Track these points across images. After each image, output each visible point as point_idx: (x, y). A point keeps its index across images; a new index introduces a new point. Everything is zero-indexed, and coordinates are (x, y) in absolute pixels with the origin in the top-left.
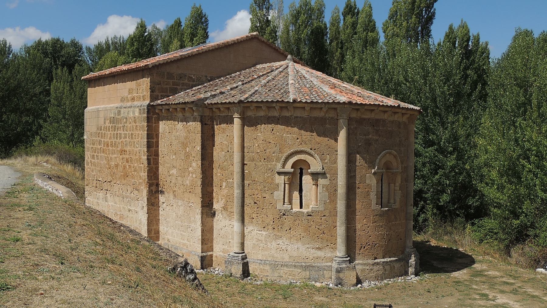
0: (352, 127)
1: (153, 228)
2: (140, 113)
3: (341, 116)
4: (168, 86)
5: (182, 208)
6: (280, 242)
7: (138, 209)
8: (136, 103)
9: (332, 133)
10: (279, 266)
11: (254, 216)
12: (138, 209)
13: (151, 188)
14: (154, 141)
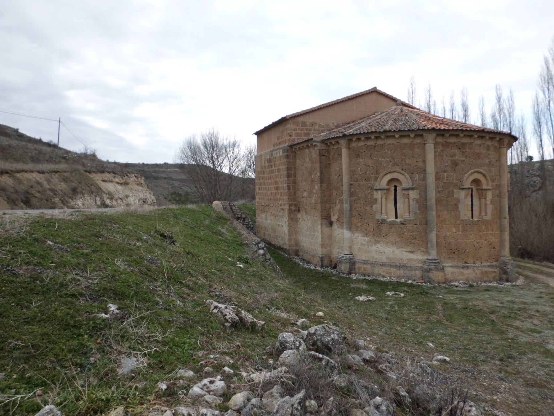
0: (439, 150)
2: (283, 153)
4: (302, 132)
5: (310, 221)
6: (378, 245)
7: (283, 224)
8: (282, 146)
11: (359, 225)
12: (283, 224)
14: (293, 172)
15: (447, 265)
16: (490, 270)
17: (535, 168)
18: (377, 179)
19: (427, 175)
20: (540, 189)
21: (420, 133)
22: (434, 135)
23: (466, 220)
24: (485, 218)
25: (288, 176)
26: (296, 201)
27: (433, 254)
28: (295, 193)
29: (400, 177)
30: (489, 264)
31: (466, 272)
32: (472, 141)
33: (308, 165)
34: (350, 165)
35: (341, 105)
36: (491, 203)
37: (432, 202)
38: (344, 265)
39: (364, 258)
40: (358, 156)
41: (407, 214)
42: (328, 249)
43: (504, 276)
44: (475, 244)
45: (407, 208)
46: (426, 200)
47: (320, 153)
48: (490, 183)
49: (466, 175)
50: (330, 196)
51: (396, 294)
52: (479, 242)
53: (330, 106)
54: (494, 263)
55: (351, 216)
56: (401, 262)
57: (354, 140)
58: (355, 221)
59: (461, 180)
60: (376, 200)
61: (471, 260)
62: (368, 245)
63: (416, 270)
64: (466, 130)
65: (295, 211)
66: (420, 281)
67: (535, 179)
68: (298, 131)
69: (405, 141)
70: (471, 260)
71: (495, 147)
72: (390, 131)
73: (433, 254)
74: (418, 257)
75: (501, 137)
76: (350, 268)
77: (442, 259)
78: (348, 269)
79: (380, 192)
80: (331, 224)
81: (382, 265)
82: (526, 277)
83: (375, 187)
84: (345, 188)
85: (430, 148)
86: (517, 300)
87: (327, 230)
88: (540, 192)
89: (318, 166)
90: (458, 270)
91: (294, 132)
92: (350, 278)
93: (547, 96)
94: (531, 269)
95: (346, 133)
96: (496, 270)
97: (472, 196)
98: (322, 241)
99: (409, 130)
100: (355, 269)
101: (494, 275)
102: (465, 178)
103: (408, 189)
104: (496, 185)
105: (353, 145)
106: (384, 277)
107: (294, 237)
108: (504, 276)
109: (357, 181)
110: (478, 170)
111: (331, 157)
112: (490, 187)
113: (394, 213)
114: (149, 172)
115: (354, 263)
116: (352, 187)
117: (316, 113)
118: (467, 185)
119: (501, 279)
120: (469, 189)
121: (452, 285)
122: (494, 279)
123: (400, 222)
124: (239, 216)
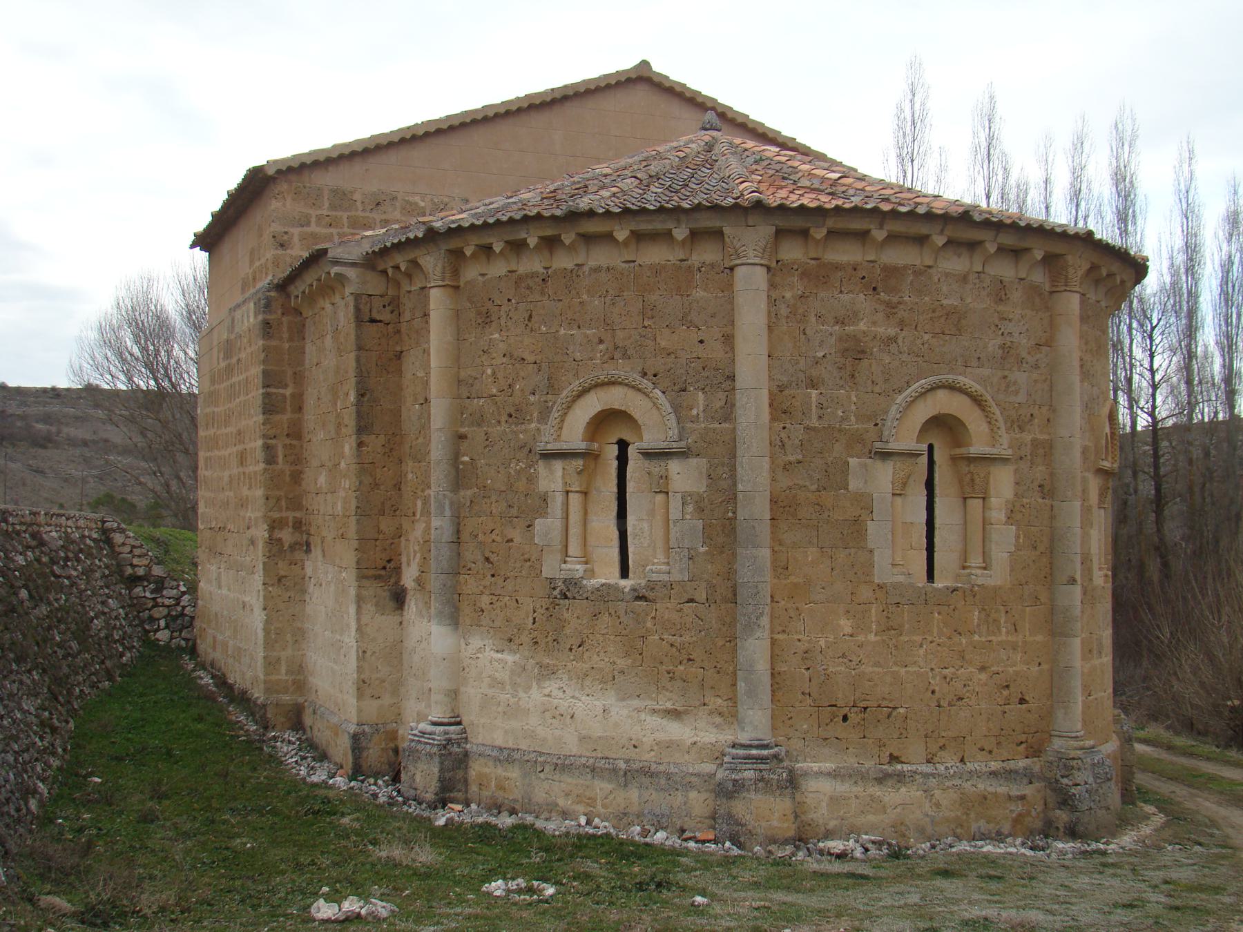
0: (788, 295)
1: (284, 655)
4: (334, 231)
6: (551, 686)
10: (547, 768)
13: (278, 534)
14: (288, 392)
15: (815, 766)
16: (1002, 790)
21: (710, 221)
23: (895, 586)
24: (981, 578)
25: (270, 407)
27: (756, 723)
28: (297, 477)
30: (994, 765)
31: (893, 796)
32: (929, 262)
33: (330, 361)
34: (457, 358)
35: (504, 128)
36: (1010, 519)
37: (755, 509)
38: (422, 766)
40: (486, 319)
41: (661, 557)
42: (387, 700)
44: (936, 683)
47: (358, 310)
50: (398, 486)
51: (530, 890)
53: (452, 128)
54: (1022, 763)
55: (457, 569)
56: (632, 753)
57: (468, 252)
60: (545, 499)
61: (915, 750)
62: (514, 685)
63: (690, 786)
64: (894, 214)
65: (292, 547)
68: (313, 228)
69: (655, 255)
70: (915, 750)
71: (1034, 289)
72: (591, 213)
73: (756, 723)
74: (693, 737)
75: (1058, 248)
76: (441, 780)
77: (796, 744)
78: (434, 785)
79: (558, 465)
80: (399, 598)
81: (563, 766)
83: (540, 447)
84: (438, 450)
85: (751, 283)
87: (383, 622)
90: (857, 789)
91: (296, 231)
92: (430, 820)
95: (438, 225)
97: (930, 485)
98: (360, 669)
99: (661, 210)
100: (466, 782)
101: (1018, 808)
103: (665, 454)
104: (1035, 443)
105: (471, 273)
106: (565, 815)
107: (289, 652)
110: (951, 377)
111: (404, 327)
112: (1002, 449)
114: (23, 417)
116: (464, 445)
117: (393, 157)
118: (906, 438)
121: (821, 852)
124: (141, 572)
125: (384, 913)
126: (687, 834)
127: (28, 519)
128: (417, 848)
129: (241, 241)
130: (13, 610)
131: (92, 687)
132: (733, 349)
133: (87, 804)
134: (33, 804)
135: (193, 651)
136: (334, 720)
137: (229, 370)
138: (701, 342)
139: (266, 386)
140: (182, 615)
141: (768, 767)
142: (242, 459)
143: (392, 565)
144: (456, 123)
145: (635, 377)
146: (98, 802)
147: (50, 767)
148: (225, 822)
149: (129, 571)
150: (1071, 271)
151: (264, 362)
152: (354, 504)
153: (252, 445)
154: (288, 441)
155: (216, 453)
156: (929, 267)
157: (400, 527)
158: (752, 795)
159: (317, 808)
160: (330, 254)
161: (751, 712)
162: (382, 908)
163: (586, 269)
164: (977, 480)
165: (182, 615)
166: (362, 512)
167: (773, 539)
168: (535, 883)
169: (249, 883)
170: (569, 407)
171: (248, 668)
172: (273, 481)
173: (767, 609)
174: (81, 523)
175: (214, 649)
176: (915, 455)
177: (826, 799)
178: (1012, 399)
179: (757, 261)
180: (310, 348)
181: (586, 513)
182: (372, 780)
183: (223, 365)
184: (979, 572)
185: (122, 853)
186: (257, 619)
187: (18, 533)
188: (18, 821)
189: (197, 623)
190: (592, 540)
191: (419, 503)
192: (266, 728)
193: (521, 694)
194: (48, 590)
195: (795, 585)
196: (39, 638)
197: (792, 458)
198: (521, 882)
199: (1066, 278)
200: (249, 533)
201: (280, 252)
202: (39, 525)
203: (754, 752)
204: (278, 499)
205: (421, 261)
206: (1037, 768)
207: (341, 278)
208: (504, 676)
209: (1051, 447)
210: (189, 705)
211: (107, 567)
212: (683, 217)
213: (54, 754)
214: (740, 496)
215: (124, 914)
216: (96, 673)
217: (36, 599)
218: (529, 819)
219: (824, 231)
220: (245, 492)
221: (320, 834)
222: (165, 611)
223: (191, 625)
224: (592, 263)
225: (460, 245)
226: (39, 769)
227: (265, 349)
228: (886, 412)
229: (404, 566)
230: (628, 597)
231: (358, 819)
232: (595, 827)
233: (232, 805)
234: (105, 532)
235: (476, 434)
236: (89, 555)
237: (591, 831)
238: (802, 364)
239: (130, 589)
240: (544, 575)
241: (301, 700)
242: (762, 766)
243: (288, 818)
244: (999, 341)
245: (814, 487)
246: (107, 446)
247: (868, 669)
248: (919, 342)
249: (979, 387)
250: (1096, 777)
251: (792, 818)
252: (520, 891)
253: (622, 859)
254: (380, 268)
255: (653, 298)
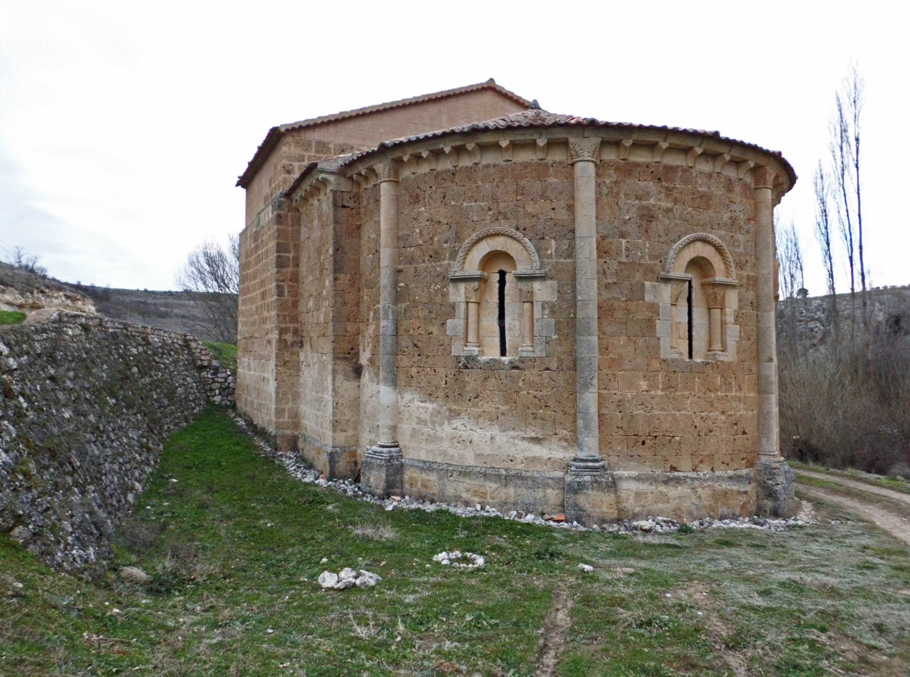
0: (608, 181)
1: (287, 407)
3: (578, 156)
6: (457, 423)
9: (561, 193)
10: (455, 474)
11: (414, 371)
13: (284, 337)
14: (291, 255)
16: (735, 488)
17: (813, 307)
18: (456, 252)
19: (578, 241)
20: (822, 341)
22: (595, 140)
23: (673, 361)
25: (281, 264)
26: (296, 321)
27: (591, 446)
28: (295, 304)
29: (512, 248)
30: (731, 473)
31: (673, 492)
32: (691, 164)
36: (736, 321)
37: (589, 312)
38: (374, 472)
39: (423, 456)
40: (416, 200)
41: (528, 342)
43: (768, 502)
44: (697, 422)
45: (528, 328)
46: (575, 305)
47: (335, 200)
48: (734, 272)
49: (675, 246)
50: (358, 304)
51: (465, 560)
52: (708, 418)
54: (745, 472)
55: (396, 351)
56: (510, 465)
58: (404, 361)
59: (661, 258)
60: (453, 307)
61: (685, 464)
62: (433, 422)
63: (546, 485)
65: (293, 344)
66: (555, 517)
67: (812, 325)
69: (525, 156)
70: (685, 464)
71: (746, 186)
72: (486, 130)
73: (591, 446)
75: (762, 161)
76: (387, 481)
77: (614, 459)
78: (382, 485)
79: (462, 286)
80: (358, 371)
81: (465, 473)
82: (818, 504)
83: (451, 275)
84: (385, 279)
85: (585, 171)
86: (808, 578)
87: (347, 386)
88: (822, 348)
89: (330, 230)
90: (653, 488)
91: (296, 164)
92: (381, 506)
93: (839, 164)
94: (822, 485)
95: (387, 142)
96: (748, 488)
98: (334, 414)
100: (402, 482)
101: (743, 499)
102: (672, 253)
103: (531, 278)
105: (406, 173)
107: (290, 405)
108: (768, 502)
109: (411, 260)
110: (704, 234)
111: (362, 211)
113: (497, 340)
114: (155, 305)
115: (400, 469)
118: (678, 271)
119: (760, 511)
120: (683, 281)
121: (635, 528)
122: (745, 511)
123: (511, 362)
124: (206, 363)
125: (372, 582)
126: (546, 516)
127: (141, 330)
128: (382, 528)
129: (263, 183)
130: (127, 378)
131: (175, 425)
132: (573, 214)
133: (166, 496)
134: (130, 497)
135: (234, 407)
136: (318, 444)
137: (257, 248)
138: (553, 209)
139: (278, 252)
140: (228, 387)
141: (599, 473)
142: (264, 296)
143: (354, 351)
144: (388, 107)
145: (512, 231)
146: (174, 495)
147: (145, 472)
148: (253, 508)
149: (199, 363)
150: (768, 176)
151: (278, 237)
152: (331, 314)
153: (270, 286)
154: (290, 283)
155: (249, 296)
156: (691, 167)
157: (358, 329)
158: (590, 492)
159: (311, 499)
160: (319, 166)
161: (587, 439)
162: (369, 578)
163: (480, 166)
164: (719, 298)
165: (228, 387)
166: (335, 320)
167: (600, 330)
168: (468, 554)
169: (271, 553)
170: (469, 250)
171: (266, 416)
172: (282, 307)
173: (596, 375)
174: (173, 335)
175: (246, 405)
176: (683, 281)
177: (633, 494)
178: (736, 250)
179: (590, 159)
180: (304, 230)
181: (479, 316)
182: (341, 481)
183: (253, 246)
184: (720, 353)
185: (186, 530)
186: (271, 387)
187: (134, 336)
188: (119, 509)
189: (237, 392)
190: (482, 333)
191: (371, 313)
192: (276, 449)
193: (438, 428)
194: (150, 369)
195: (613, 360)
196: (143, 396)
197: (610, 281)
198: (457, 553)
199: (765, 180)
200: (267, 337)
201: (287, 176)
202: (148, 334)
203: (590, 464)
204: (285, 317)
205: (374, 167)
206: (752, 474)
207: (325, 182)
208: (427, 417)
209: (756, 280)
210: (231, 436)
211: (187, 360)
212: (544, 131)
213: (148, 464)
214: (579, 303)
215: (183, 582)
216: (178, 418)
217: (143, 374)
218: (444, 506)
219: (631, 142)
220: (265, 314)
221: (315, 517)
222: (218, 385)
223: (233, 393)
224: (484, 162)
225: (401, 155)
226: (137, 474)
227: (278, 230)
228: (667, 254)
229: (361, 353)
230: (507, 367)
231: (337, 507)
232: (488, 512)
233: (257, 497)
234: (186, 341)
235: (410, 269)
236: (176, 353)
237: (485, 514)
238: (616, 224)
239: (200, 373)
240: (453, 354)
241: (296, 433)
242: (596, 473)
243: (293, 505)
244: (729, 215)
245: (624, 299)
246: (194, 318)
247: (656, 412)
248: (685, 212)
249: (720, 241)
250: (787, 480)
251: (615, 506)
252: (458, 560)
253: (516, 535)
254: (349, 175)
255: (523, 182)
